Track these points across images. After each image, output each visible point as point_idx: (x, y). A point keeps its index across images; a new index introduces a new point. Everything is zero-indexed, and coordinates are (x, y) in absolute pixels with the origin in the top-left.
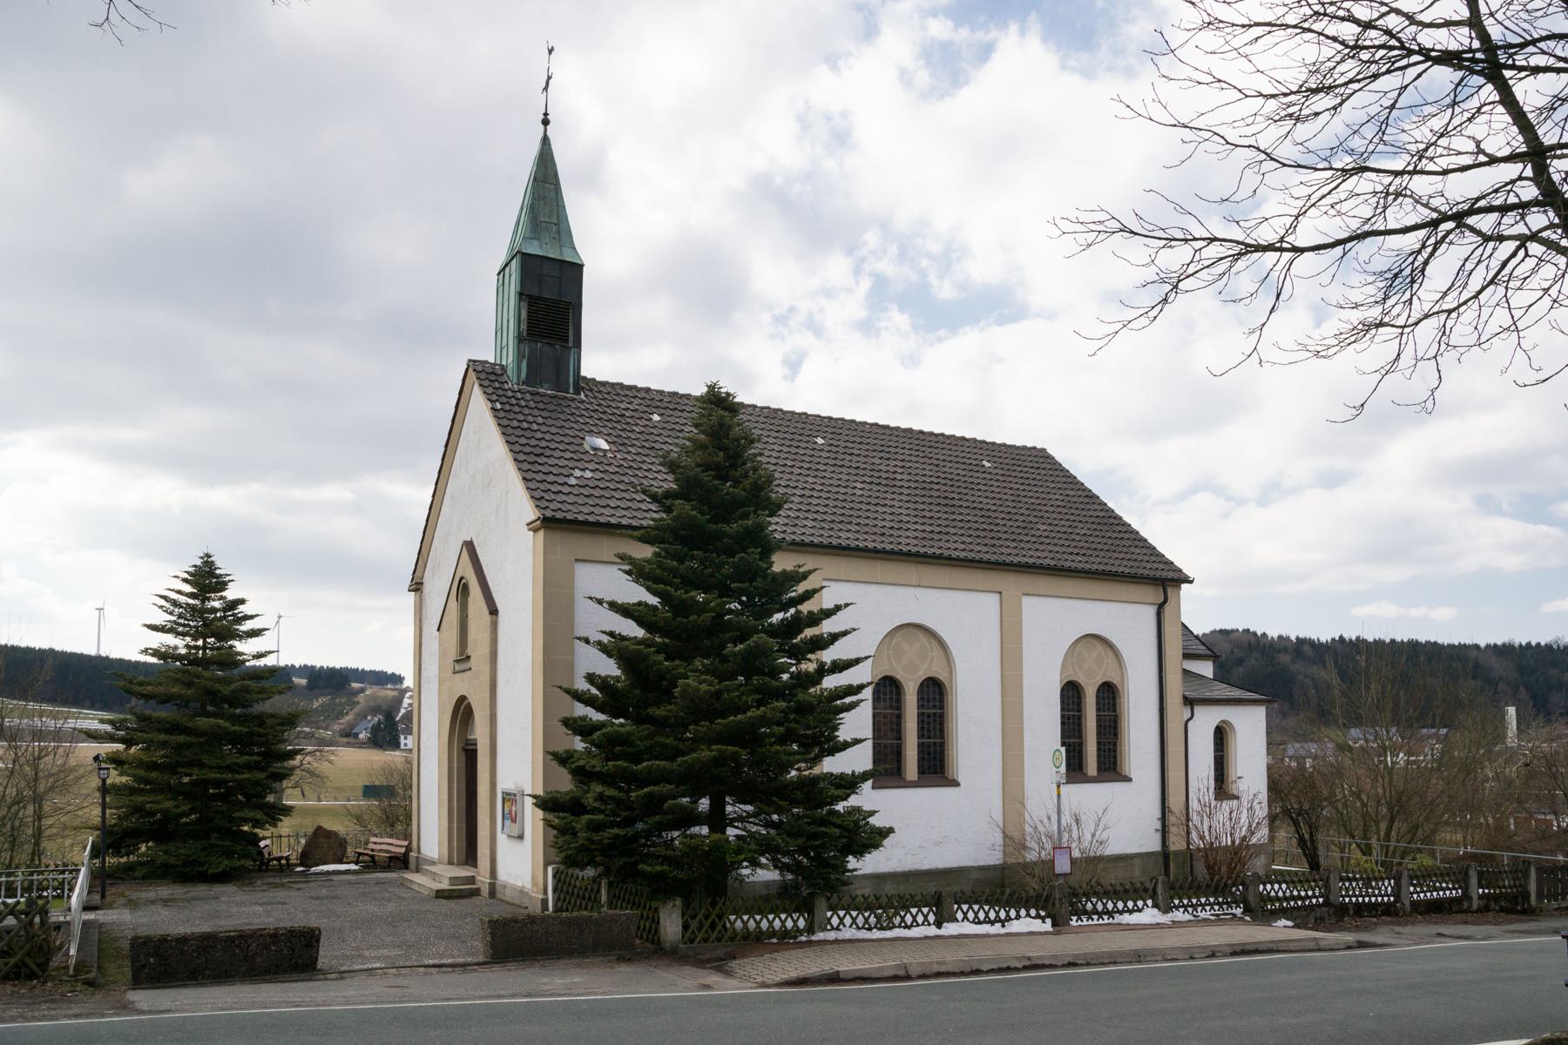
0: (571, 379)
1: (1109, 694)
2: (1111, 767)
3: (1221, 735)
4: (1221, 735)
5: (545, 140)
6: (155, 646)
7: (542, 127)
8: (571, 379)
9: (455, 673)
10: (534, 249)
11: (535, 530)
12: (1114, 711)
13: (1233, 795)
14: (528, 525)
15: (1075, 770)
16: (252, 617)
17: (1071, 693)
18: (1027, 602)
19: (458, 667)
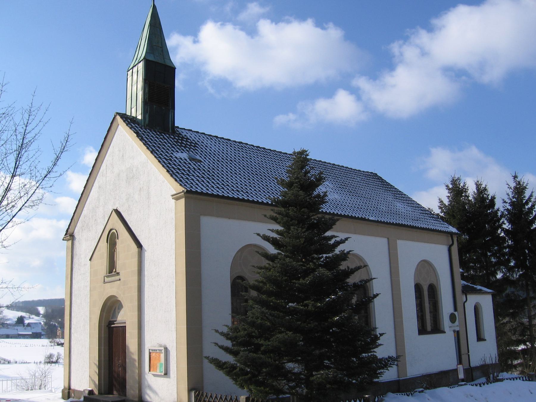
0: (170, 126)
1: (433, 290)
2: (437, 329)
3: (477, 310)
4: (477, 310)
5: (154, 5)
6: (215, 356)
7: (32, 123)
8: (170, 126)
9: (105, 282)
10: (151, 58)
11: (177, 199)
12: (434, 298)
13: (482, 339)
14: (172, 196)
15: (422, 331)
16: (352, 251)
17: (418, 288)
18: (400, 243)
19: (107, 279)
